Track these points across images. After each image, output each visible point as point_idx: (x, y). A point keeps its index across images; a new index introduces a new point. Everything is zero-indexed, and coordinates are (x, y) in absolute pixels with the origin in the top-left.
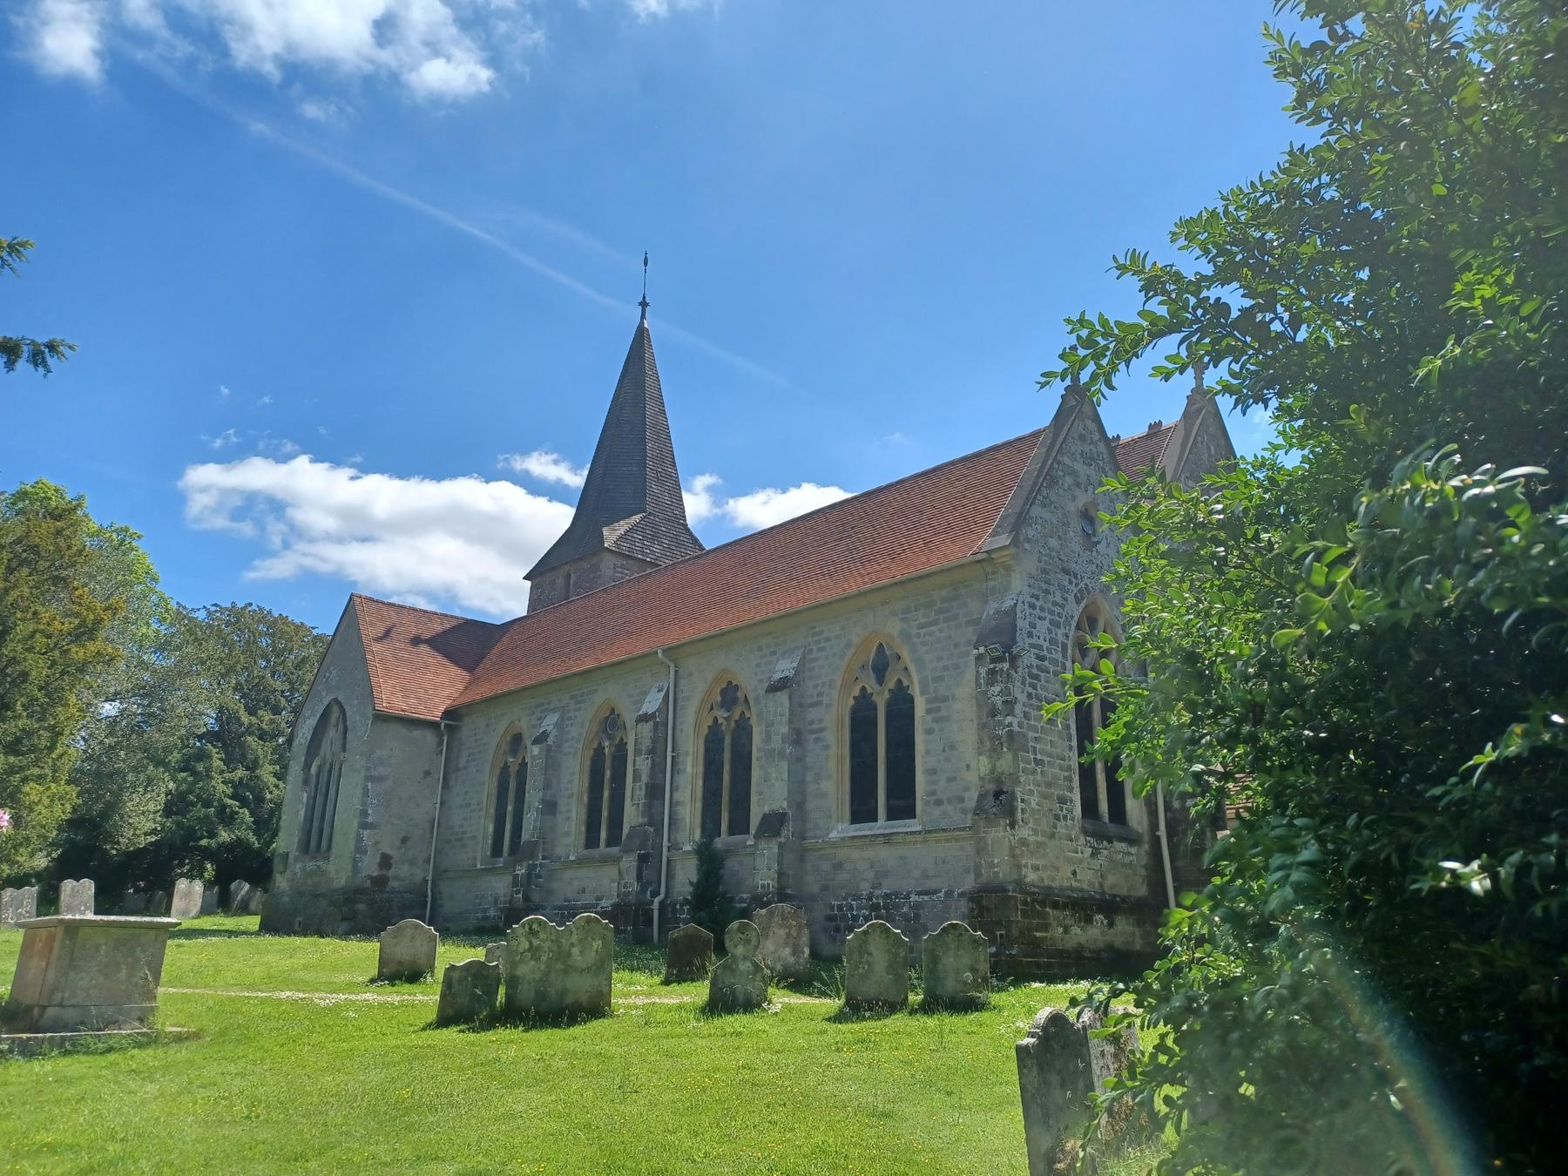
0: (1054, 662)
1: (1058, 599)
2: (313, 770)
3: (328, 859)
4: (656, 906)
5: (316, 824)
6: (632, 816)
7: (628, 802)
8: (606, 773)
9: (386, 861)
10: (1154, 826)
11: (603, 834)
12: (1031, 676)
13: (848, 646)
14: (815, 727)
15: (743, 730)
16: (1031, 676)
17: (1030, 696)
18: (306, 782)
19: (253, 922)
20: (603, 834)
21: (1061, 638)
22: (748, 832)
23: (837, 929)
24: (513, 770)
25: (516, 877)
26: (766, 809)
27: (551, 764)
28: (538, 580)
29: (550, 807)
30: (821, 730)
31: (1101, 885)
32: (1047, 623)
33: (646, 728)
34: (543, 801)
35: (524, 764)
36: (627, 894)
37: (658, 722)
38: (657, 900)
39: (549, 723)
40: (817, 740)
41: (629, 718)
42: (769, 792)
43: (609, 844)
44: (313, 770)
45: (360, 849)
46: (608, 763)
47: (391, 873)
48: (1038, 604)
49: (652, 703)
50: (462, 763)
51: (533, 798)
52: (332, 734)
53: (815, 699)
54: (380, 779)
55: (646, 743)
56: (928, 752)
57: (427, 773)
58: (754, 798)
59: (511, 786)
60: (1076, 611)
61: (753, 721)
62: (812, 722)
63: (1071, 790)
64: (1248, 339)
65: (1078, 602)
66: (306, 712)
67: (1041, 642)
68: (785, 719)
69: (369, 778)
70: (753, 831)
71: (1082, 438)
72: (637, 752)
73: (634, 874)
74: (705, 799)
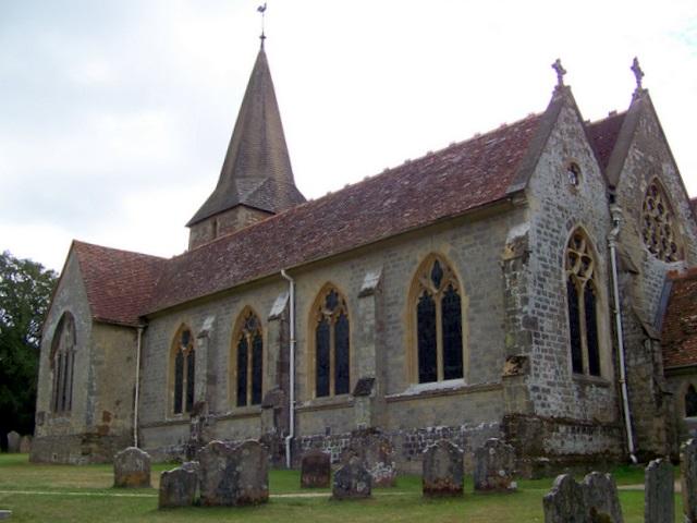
0: (553, 269)
1: (557, 228)
2: (56, 357)
3: (69, 415)
4: (287, 443)
5: (61, 391)
6: (268, 383)
7: (265, 374)
8: (249, 354)
9: (107, 417)
10: (617, 375)
11: (249, 397)
12: (540, 279)
13: (415, 262)
14: (393, 319)
15: (342, 324)
16: (540, 279)
17: (539, 293)
18: (53, 366)
19: (24, 457)
20: (249, 397)
21: (558, 254)
22: (348, 392)
23: (412, 452)
24: (185, 355)
25: (192, 426)
26: (361, 376)
27: (212, 355)
28: (195, 228)
29: (212, 380)
30: (396, 322)
31: (585, 415)
32: (549, 243)
33: (275, 325)
34: (208, 376)
35: (192, 352)
36: (268, 435)
37: (283, 319)
38: (288, 438)
39: (208, 324)
40: (394, 328)
41: (263, 317)
42: (363, 362)
43: (253, 403)
44: (56, 357)
45: (89, 406)
46: (250, 348)
47: (110, 424)
48: (543, 231)
49: (277, 309)
50: (152, 352)
51: (201, 371)
52: (66, 333)
53: (392, 300)
54: (100, 363)
55: (276, 334)
56: (471, 333)
57: (129, 359)
58: (352, 370)
59: (184, 366)
60: (568, 235)
61: (350, 317)
62: (390, 317)
63: (566, 353)
64: (119, 453)
65: (569, 229)
66: (50, 320)
67: (546, 256)
68: (373, 315)
69: (93, 362)
70: (352, 391)
71: (567, 120)
72: (269, 340)
73: (272, 421)
74: (318, 371)
